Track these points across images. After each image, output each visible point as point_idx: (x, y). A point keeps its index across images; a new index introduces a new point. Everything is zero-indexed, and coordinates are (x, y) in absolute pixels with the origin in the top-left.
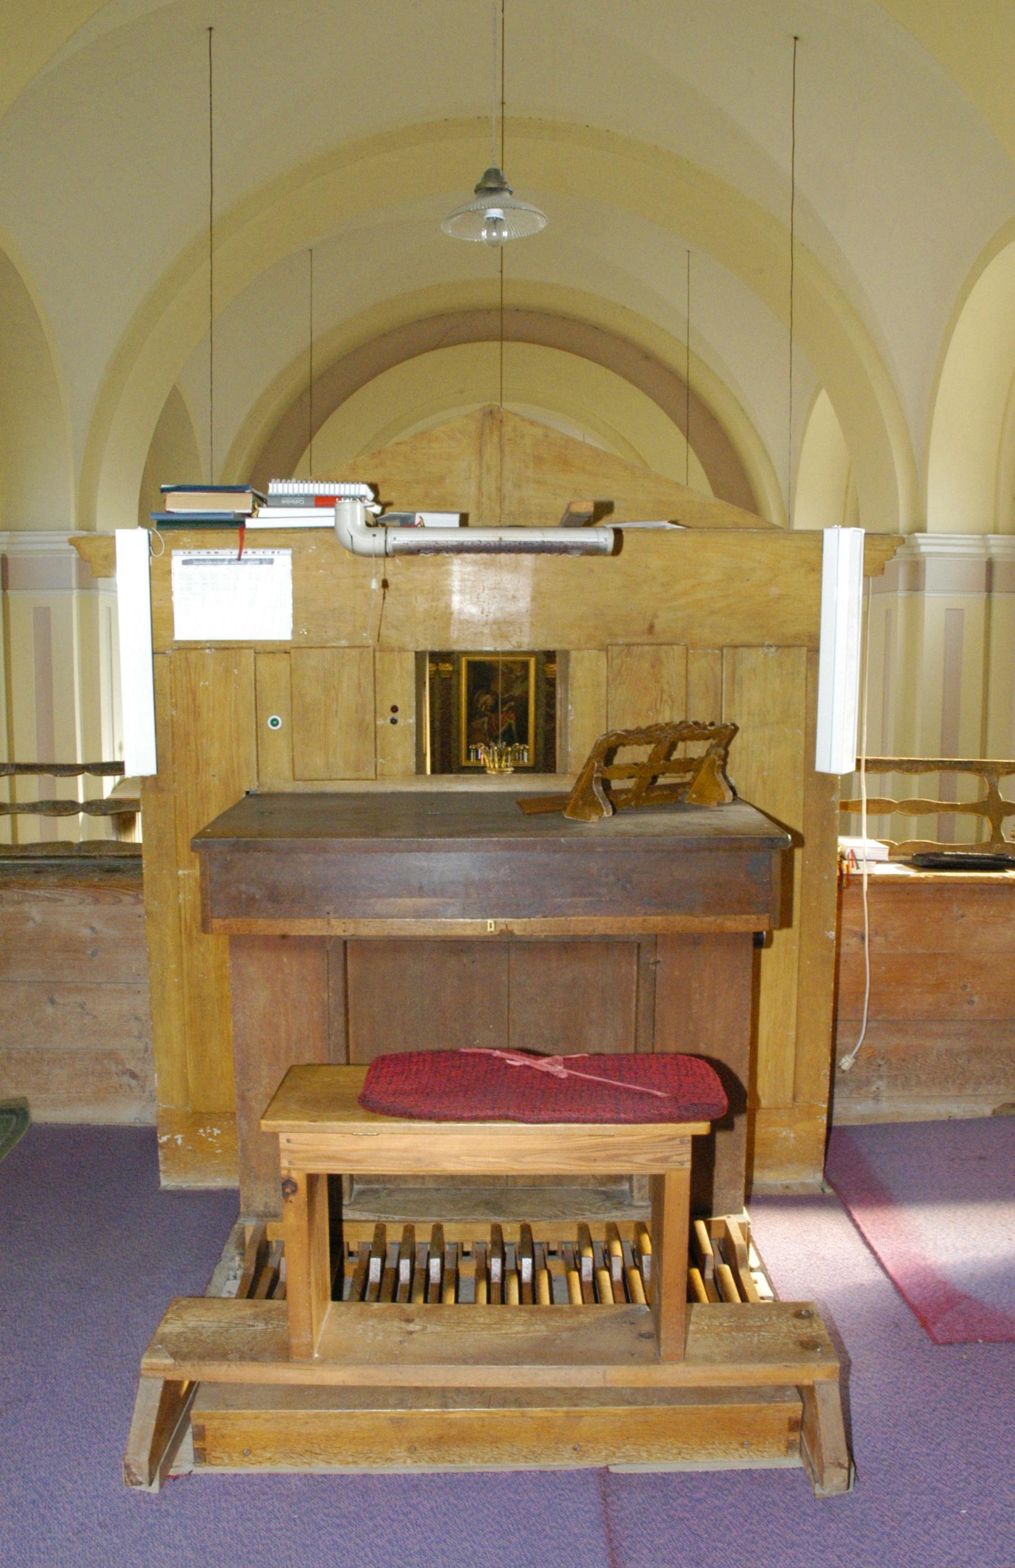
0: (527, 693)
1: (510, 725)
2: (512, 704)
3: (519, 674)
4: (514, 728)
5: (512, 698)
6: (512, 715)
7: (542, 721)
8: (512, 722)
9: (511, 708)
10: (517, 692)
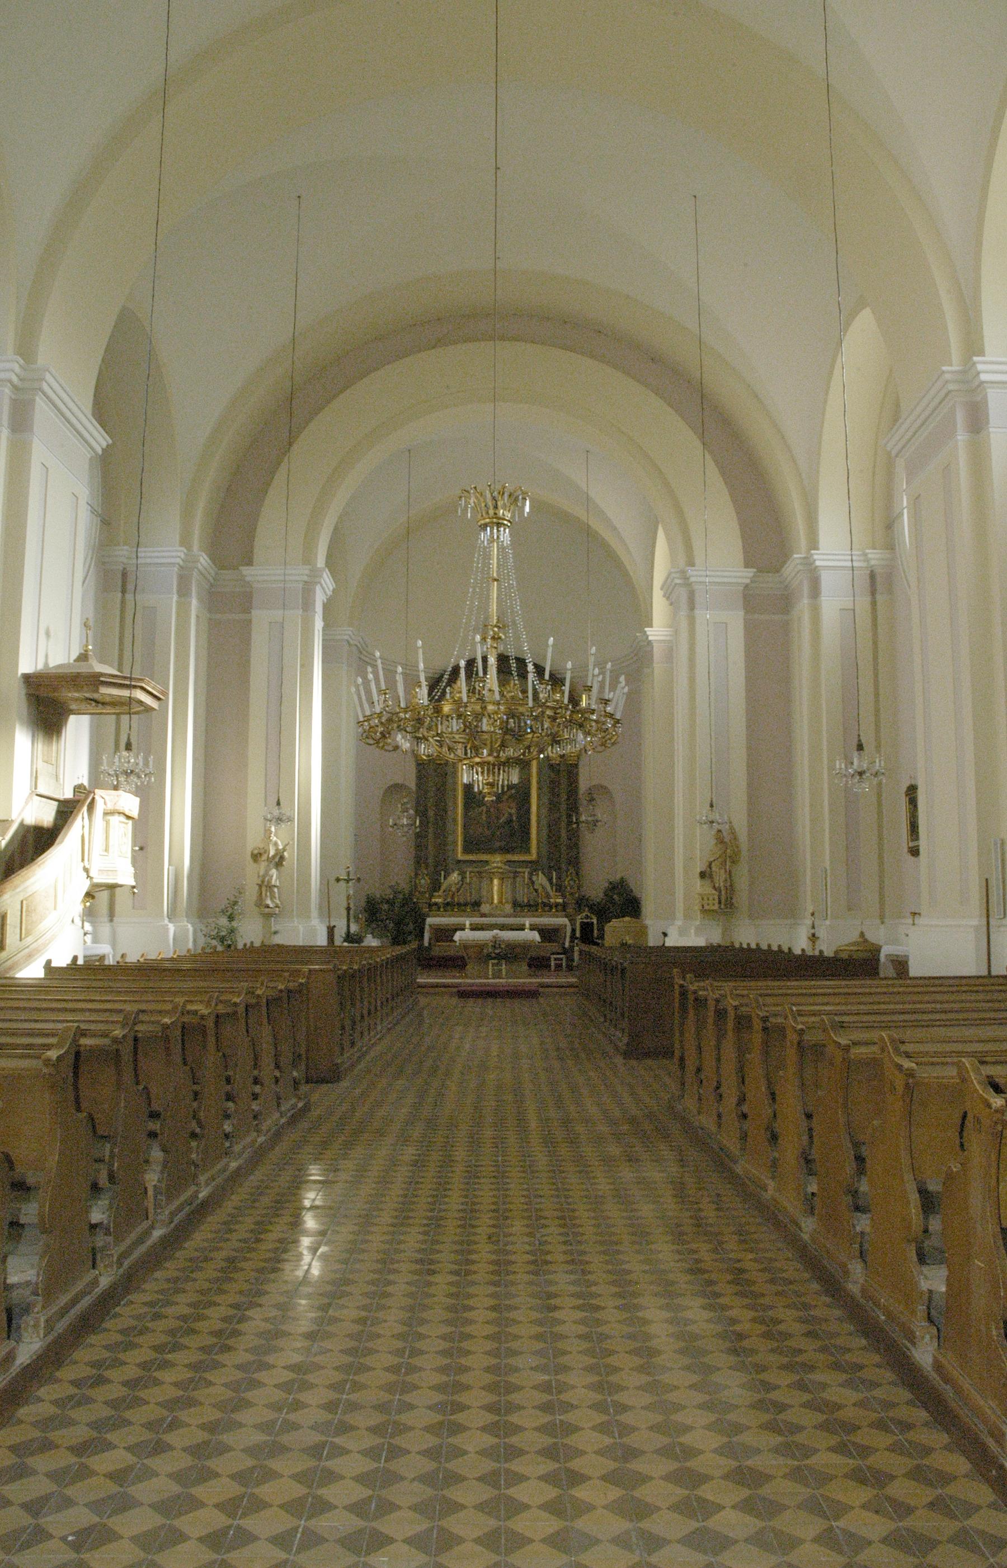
6: (513, 805)
7: (544, 811)
8: (513, 811)
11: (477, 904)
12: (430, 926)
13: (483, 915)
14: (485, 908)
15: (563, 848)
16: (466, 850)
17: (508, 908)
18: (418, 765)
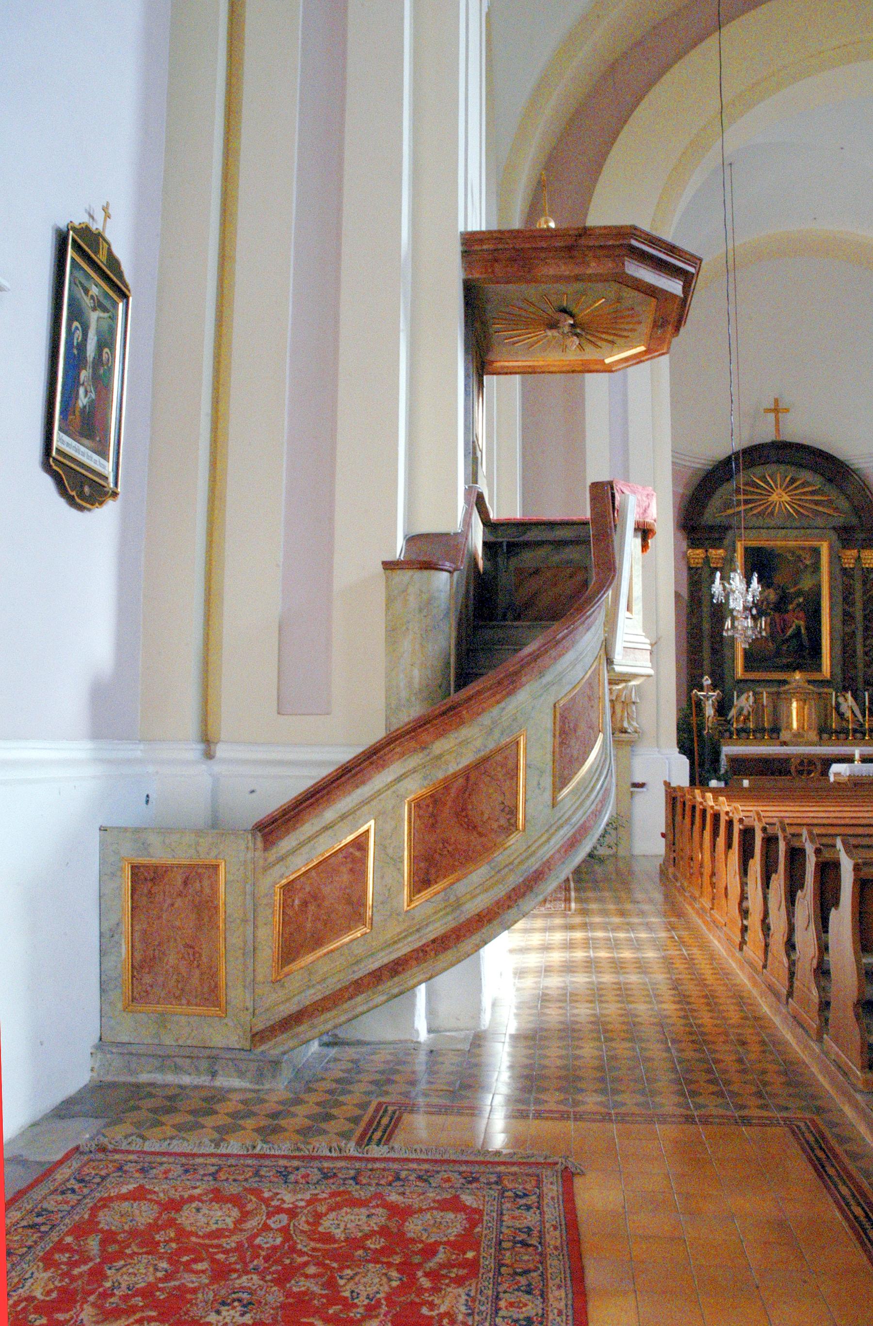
0: (819, 586)
1: (798, 628)
2: (801, 600)
3: (808, 562)
4: (803, 631)
5: (799, 593)
6: (801, 615)
8: (802, 623)
9: (799, 605)
10: (806, 584)
11: (775, 730)
12: (726, 756)
13: (785, 744)
14: (785, 735)
15: (860, 666)
16: (747, 668)
17: (813, 735)
18: (690, 569)
